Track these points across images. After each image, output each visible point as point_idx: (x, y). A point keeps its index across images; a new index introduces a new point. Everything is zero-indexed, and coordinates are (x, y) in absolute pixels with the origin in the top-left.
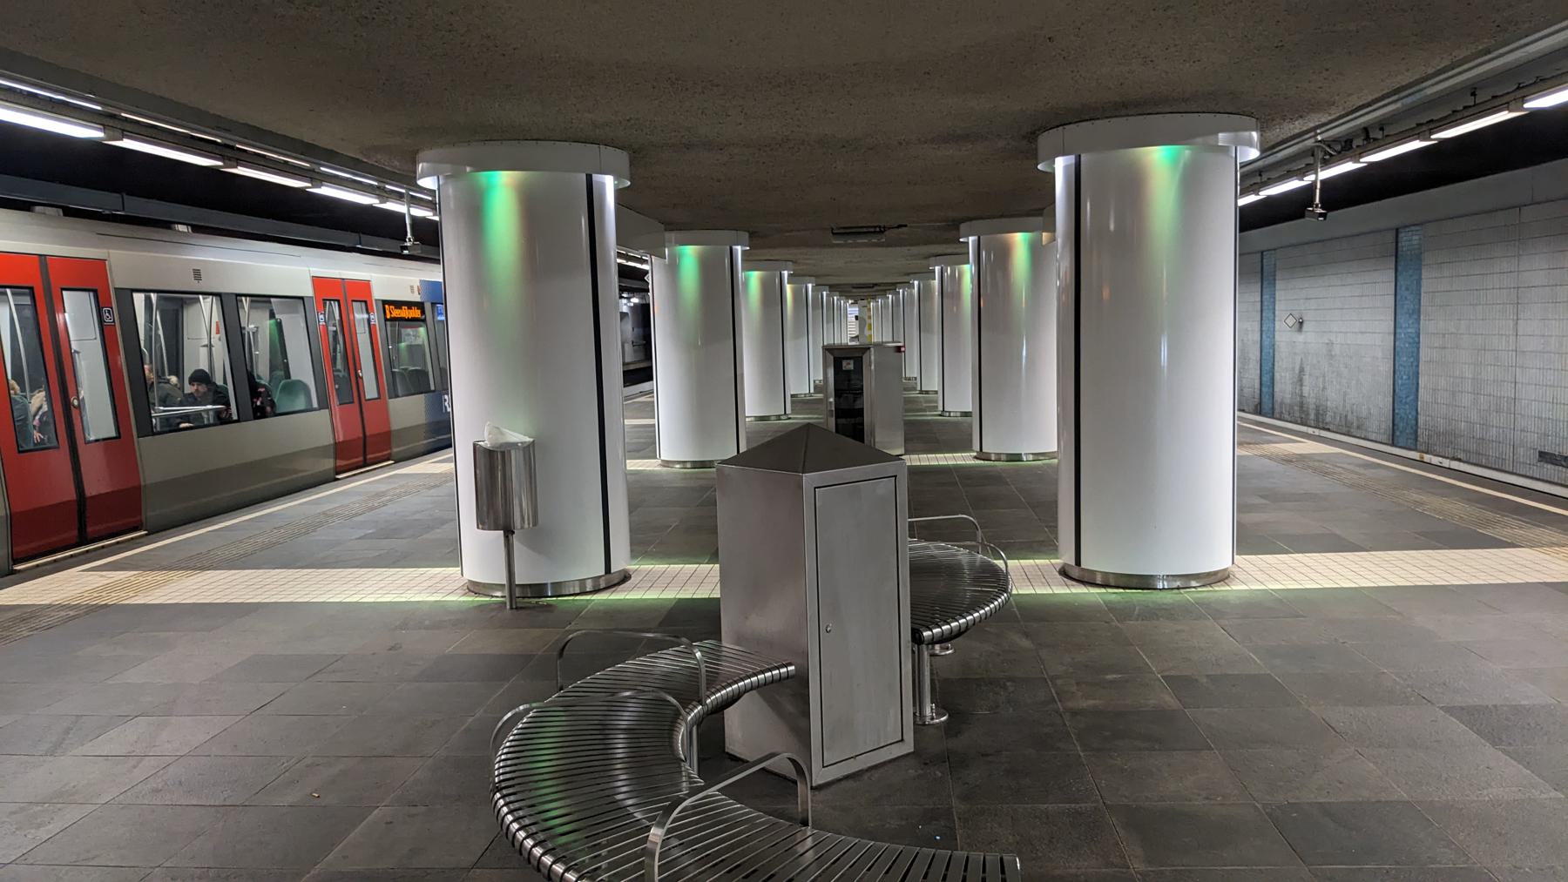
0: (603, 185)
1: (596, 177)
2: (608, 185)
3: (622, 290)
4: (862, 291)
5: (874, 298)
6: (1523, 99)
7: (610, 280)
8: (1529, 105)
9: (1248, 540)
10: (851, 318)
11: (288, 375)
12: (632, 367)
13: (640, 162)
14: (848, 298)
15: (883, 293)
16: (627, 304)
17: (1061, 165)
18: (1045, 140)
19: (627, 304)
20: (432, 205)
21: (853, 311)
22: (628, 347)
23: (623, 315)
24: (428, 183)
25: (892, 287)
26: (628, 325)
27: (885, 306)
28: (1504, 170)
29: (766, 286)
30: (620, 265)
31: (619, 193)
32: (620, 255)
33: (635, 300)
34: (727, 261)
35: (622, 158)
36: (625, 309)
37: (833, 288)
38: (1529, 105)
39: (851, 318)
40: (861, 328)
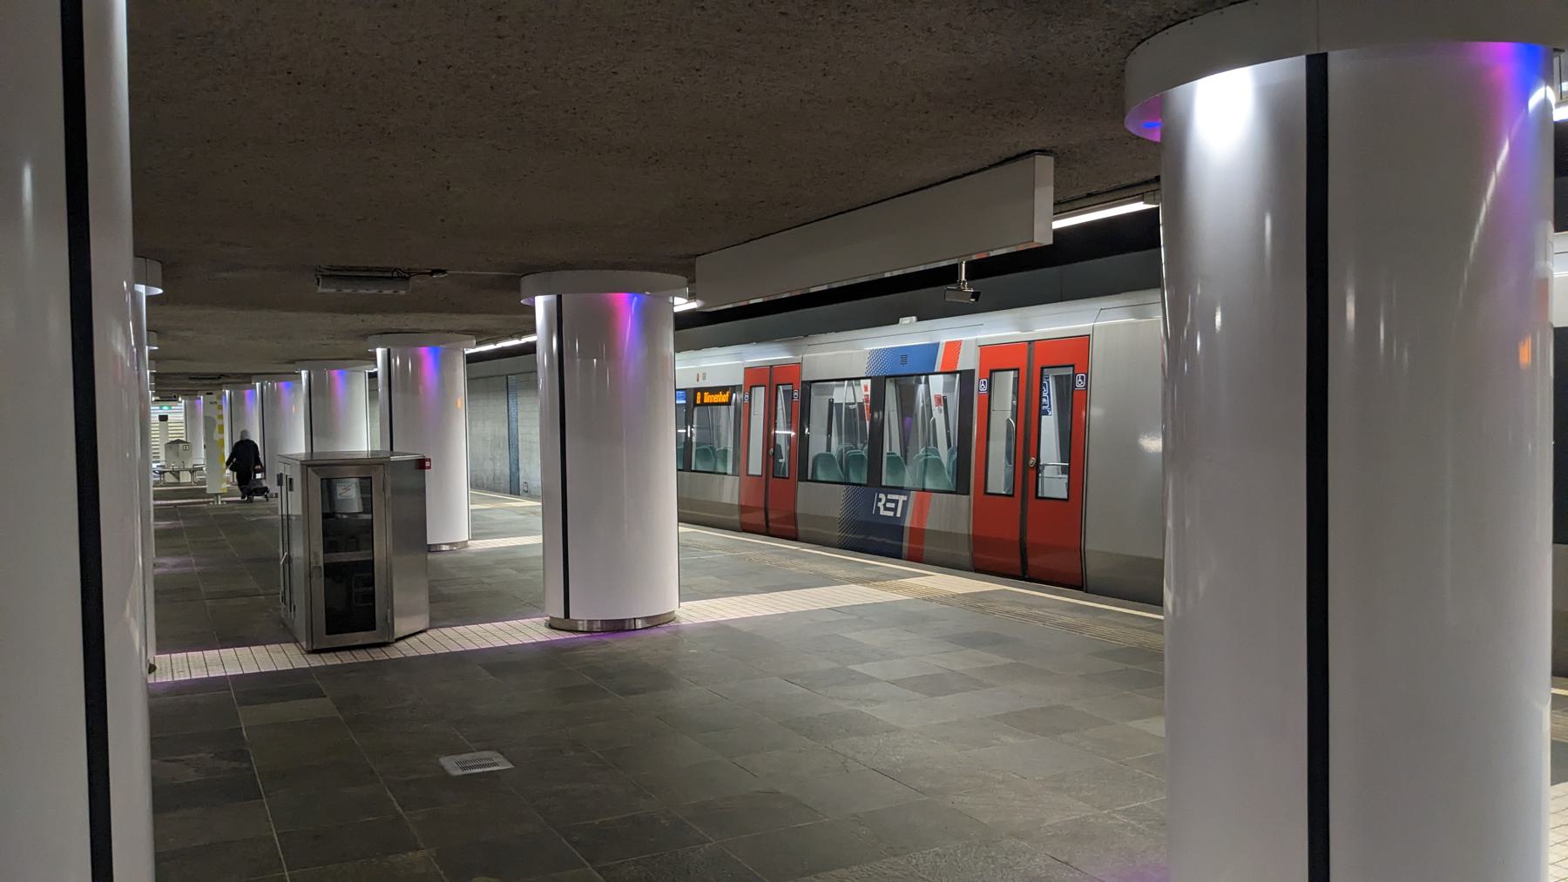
11: (734, 389)
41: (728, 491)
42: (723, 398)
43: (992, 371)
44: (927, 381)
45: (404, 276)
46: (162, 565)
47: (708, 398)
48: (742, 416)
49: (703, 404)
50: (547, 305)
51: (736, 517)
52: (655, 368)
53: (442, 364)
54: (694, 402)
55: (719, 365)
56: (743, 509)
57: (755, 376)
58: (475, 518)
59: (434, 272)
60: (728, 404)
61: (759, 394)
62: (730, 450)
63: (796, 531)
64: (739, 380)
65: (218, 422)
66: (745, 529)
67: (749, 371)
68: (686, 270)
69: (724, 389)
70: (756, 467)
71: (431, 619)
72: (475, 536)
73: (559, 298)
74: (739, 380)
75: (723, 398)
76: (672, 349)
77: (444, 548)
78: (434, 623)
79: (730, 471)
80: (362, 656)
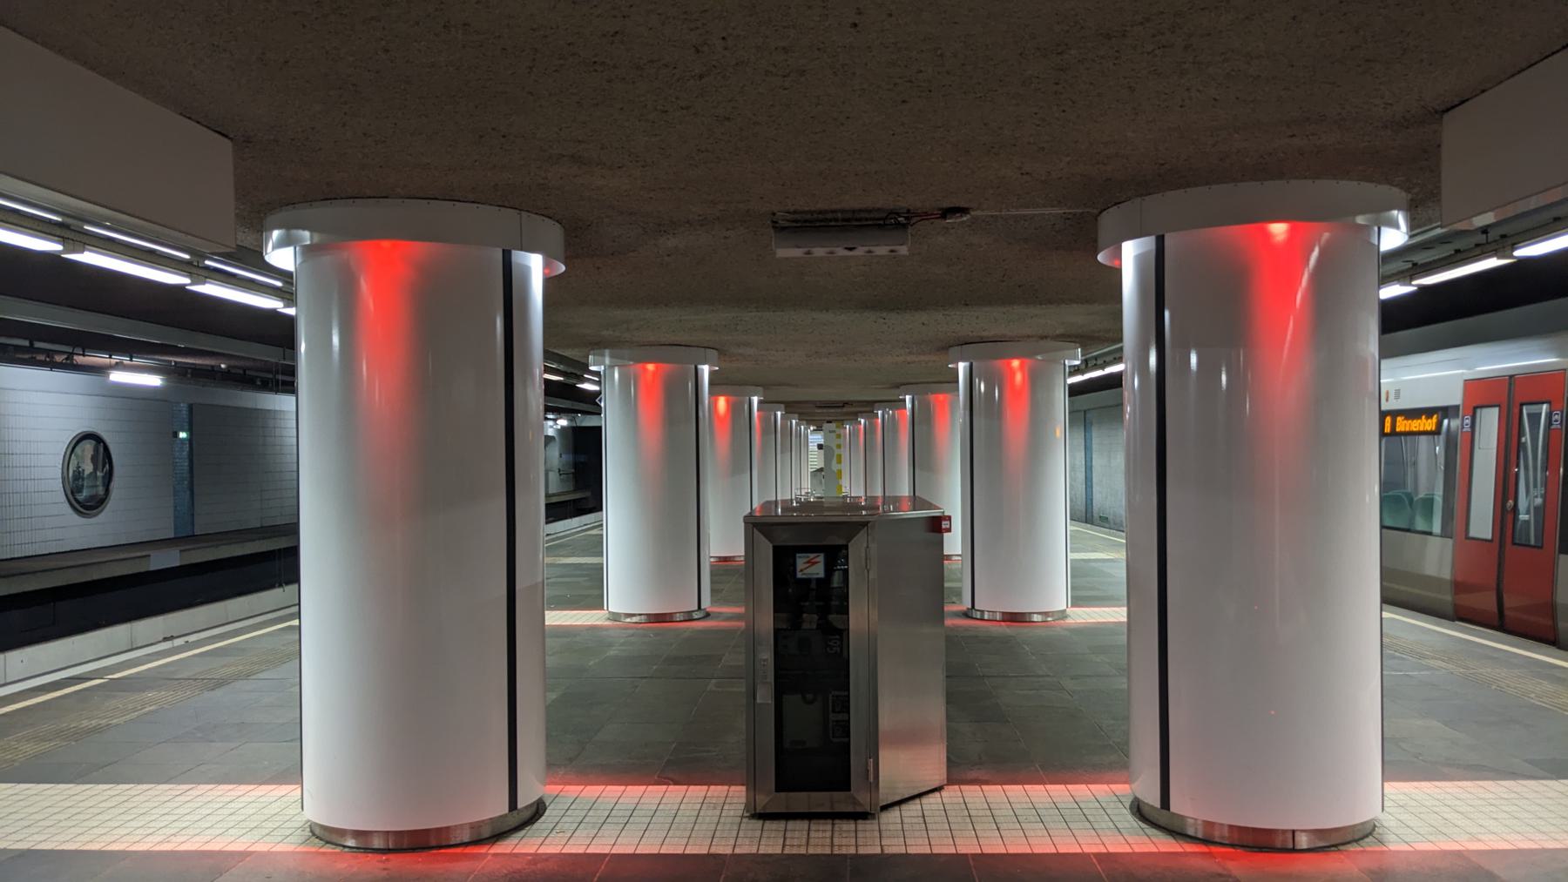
0: (526, 271)
1: (519, 257)
2: (534, 266)
3: (548, 409)
4: (829, 412)
5: (841, 422)
6: (1514, 247)
7: (532, 396)
8: (1521, 253)
9: (1077, 601)
10: (813, 447)
11: (1446, 412)
12: (554, 500)
13: (578, 246)
14: (809, 422)
15: (854, 417)
16: (556, 425)
17: (1131, 252)
18: (1109, 220)
19: (556, 425)
20: (287, 295)
21: (816, 439)
22: (553, 476)
23: (549, 439)
24: (282, 257)
25: (868, 407)
26: (555, 452)
27: (854, 434)
28: (271, 587)
29: (734, 409)
30: (547, 382)
31: (549, 283)
32: (547, 370)
33: (563, 422)
34: (691, 385)
35: (554, 232)
36: (550, 432)
37: (791, 407)
38: (1521, 253)
39: (813, 447)
40: (828, 460)
41: (1436, 558)
42: (1428, 424)
43: (1475, 408)
44: (1395, 414)
45: (890, 222)
46: (718, 616)
47: (1403, 425)
48: (1458, 454)
49: (1394, 433)
50: (1140, 260)
51: (1448, 598)
52: (1332, 380)
53: (1037, 380)
54: (1394, 429)
55: (1432, 377)
56: (1459, 587)
57: (1481, 393)
58: (1078, 572)
59: (947, 212)
60: (1437, 432)
61: (1490, 420)
62: (1439, 499)
63: (1554, 628)
64: (1455, 398)
65: (837, 452)
66: (1461, 615)
67: (1471, 386)
68: (1416, 179)
69: (1428, 412)
70: (1482, 524)
71: (950, 763)
72: (1077, 601)
73: (1160, 241)
74: (1455, 398)
75: (1428, 424)
76: (1373, 346)
77: (1036, 618)
78: (960, 770)
79: (1437, 528)
80: (1521, 207)
